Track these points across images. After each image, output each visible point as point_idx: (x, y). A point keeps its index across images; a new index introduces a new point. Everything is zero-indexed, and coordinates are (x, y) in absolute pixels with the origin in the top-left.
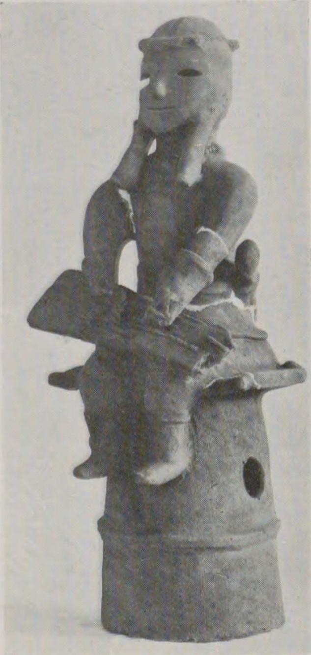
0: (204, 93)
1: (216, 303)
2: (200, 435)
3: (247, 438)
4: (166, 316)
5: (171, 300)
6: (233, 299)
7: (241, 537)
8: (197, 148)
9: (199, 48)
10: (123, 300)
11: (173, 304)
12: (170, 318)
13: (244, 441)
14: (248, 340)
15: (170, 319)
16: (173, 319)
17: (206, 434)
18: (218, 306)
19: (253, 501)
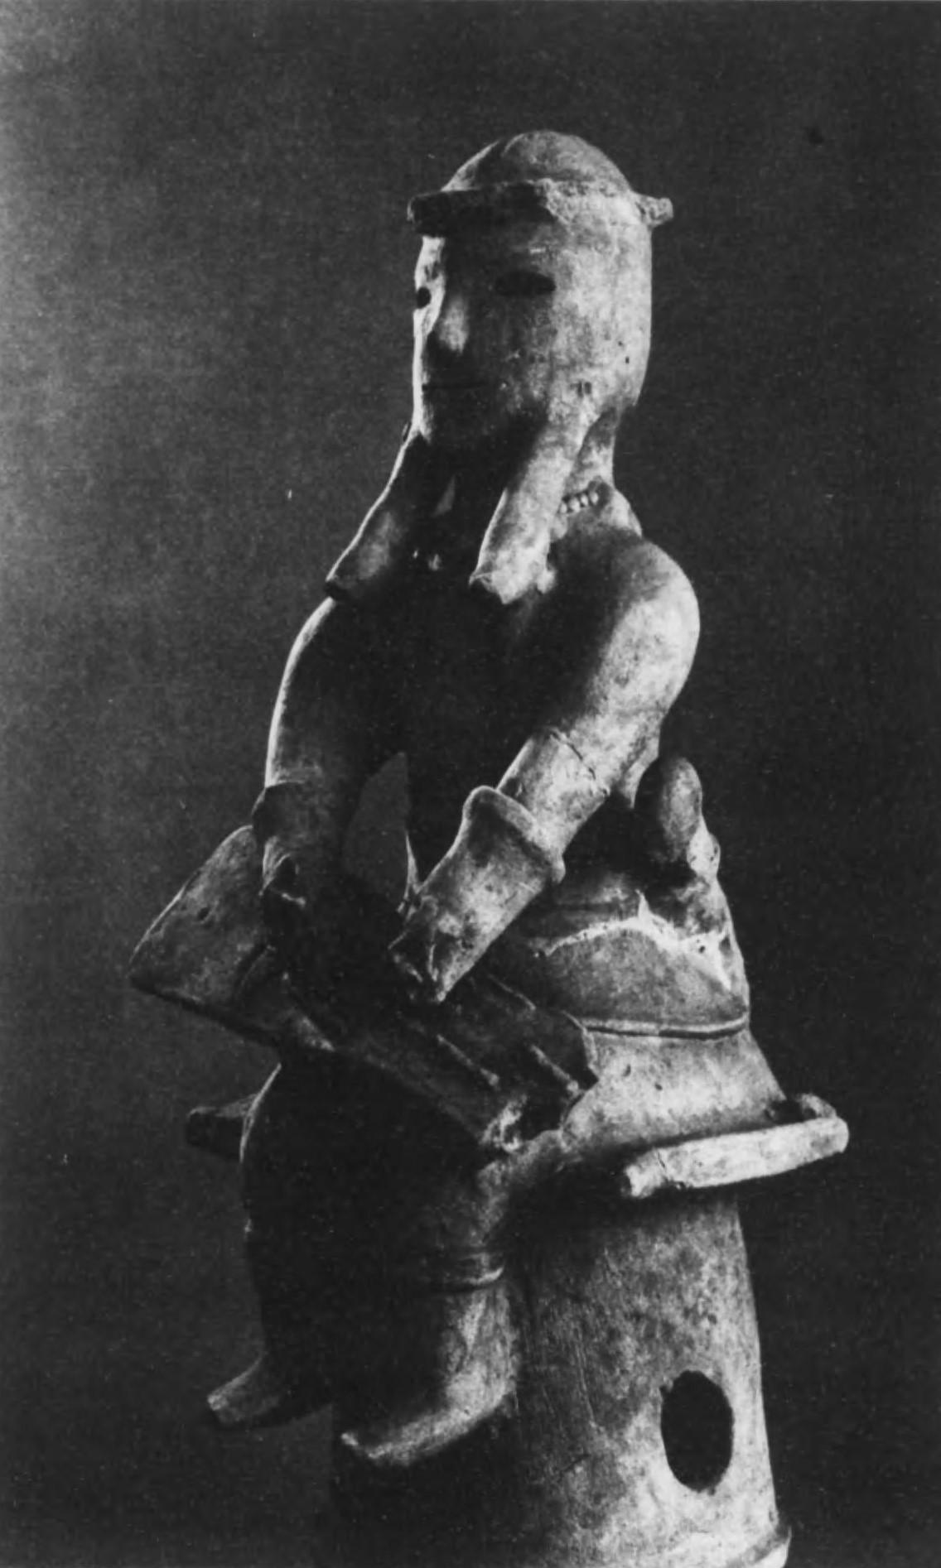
0: (563, 342)
1: (595, 930)
2: (539, 1311)
3: (678, 1319)
4: (427, 976)
5: (439, 933)
6: (645, 922)
7: (478, 1316)
8: (645, 239)
9: (551, 220)
10: (307, 803)
11: (446, 944)
12: (439, 984)
13: (669, 1328)
14: (676, 1041)
15: (433, 986)
16: (448, 983)
17: (93, 810)
18: (598, 941)
19: (693, 1503)
